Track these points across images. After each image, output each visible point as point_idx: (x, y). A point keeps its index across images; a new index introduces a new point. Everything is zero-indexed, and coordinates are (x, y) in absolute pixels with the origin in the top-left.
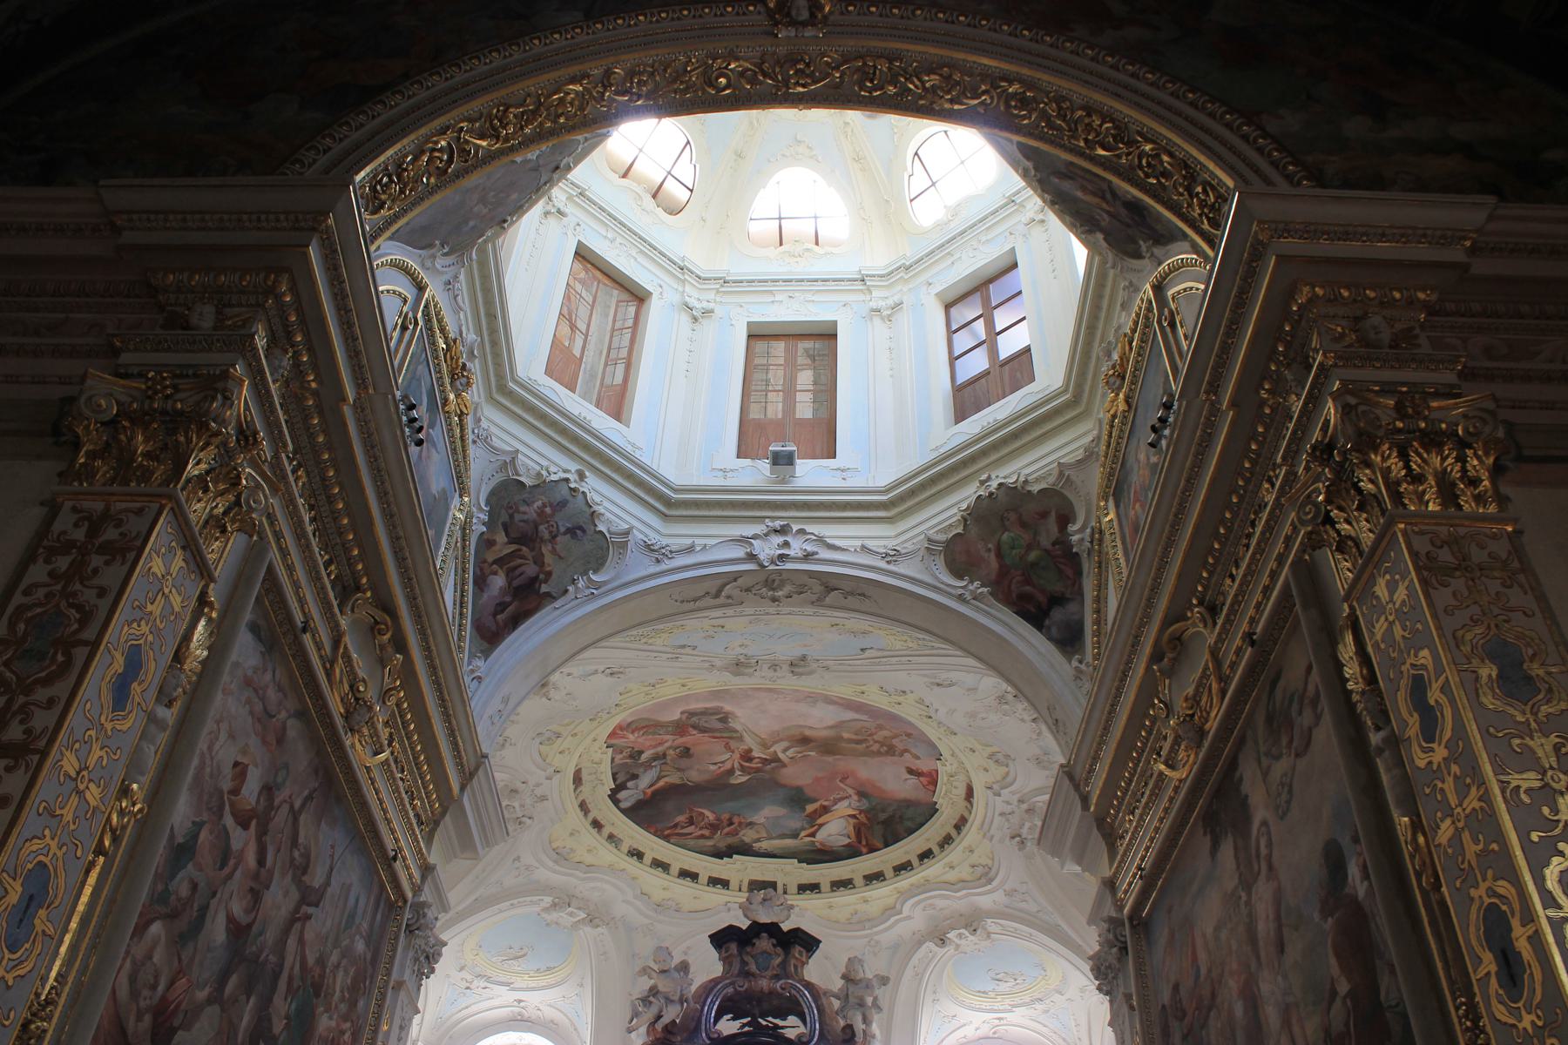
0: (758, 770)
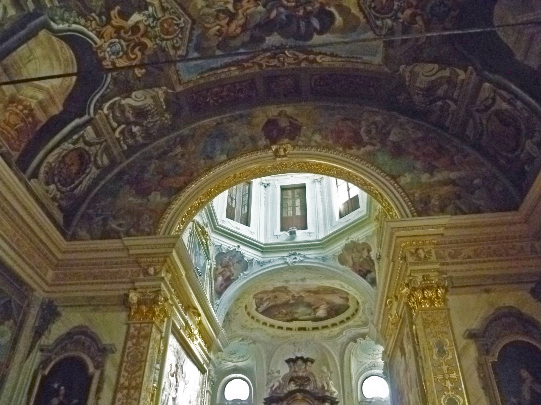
0: (297, 299)
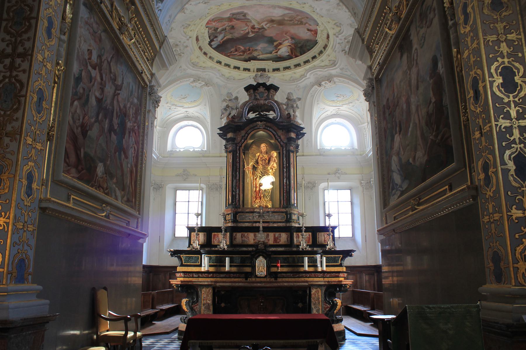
0: (257, 32)
